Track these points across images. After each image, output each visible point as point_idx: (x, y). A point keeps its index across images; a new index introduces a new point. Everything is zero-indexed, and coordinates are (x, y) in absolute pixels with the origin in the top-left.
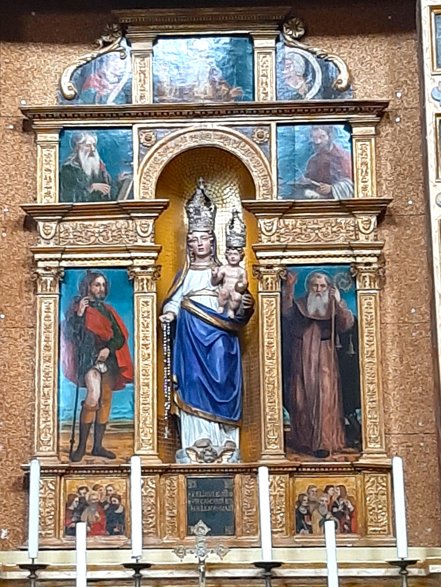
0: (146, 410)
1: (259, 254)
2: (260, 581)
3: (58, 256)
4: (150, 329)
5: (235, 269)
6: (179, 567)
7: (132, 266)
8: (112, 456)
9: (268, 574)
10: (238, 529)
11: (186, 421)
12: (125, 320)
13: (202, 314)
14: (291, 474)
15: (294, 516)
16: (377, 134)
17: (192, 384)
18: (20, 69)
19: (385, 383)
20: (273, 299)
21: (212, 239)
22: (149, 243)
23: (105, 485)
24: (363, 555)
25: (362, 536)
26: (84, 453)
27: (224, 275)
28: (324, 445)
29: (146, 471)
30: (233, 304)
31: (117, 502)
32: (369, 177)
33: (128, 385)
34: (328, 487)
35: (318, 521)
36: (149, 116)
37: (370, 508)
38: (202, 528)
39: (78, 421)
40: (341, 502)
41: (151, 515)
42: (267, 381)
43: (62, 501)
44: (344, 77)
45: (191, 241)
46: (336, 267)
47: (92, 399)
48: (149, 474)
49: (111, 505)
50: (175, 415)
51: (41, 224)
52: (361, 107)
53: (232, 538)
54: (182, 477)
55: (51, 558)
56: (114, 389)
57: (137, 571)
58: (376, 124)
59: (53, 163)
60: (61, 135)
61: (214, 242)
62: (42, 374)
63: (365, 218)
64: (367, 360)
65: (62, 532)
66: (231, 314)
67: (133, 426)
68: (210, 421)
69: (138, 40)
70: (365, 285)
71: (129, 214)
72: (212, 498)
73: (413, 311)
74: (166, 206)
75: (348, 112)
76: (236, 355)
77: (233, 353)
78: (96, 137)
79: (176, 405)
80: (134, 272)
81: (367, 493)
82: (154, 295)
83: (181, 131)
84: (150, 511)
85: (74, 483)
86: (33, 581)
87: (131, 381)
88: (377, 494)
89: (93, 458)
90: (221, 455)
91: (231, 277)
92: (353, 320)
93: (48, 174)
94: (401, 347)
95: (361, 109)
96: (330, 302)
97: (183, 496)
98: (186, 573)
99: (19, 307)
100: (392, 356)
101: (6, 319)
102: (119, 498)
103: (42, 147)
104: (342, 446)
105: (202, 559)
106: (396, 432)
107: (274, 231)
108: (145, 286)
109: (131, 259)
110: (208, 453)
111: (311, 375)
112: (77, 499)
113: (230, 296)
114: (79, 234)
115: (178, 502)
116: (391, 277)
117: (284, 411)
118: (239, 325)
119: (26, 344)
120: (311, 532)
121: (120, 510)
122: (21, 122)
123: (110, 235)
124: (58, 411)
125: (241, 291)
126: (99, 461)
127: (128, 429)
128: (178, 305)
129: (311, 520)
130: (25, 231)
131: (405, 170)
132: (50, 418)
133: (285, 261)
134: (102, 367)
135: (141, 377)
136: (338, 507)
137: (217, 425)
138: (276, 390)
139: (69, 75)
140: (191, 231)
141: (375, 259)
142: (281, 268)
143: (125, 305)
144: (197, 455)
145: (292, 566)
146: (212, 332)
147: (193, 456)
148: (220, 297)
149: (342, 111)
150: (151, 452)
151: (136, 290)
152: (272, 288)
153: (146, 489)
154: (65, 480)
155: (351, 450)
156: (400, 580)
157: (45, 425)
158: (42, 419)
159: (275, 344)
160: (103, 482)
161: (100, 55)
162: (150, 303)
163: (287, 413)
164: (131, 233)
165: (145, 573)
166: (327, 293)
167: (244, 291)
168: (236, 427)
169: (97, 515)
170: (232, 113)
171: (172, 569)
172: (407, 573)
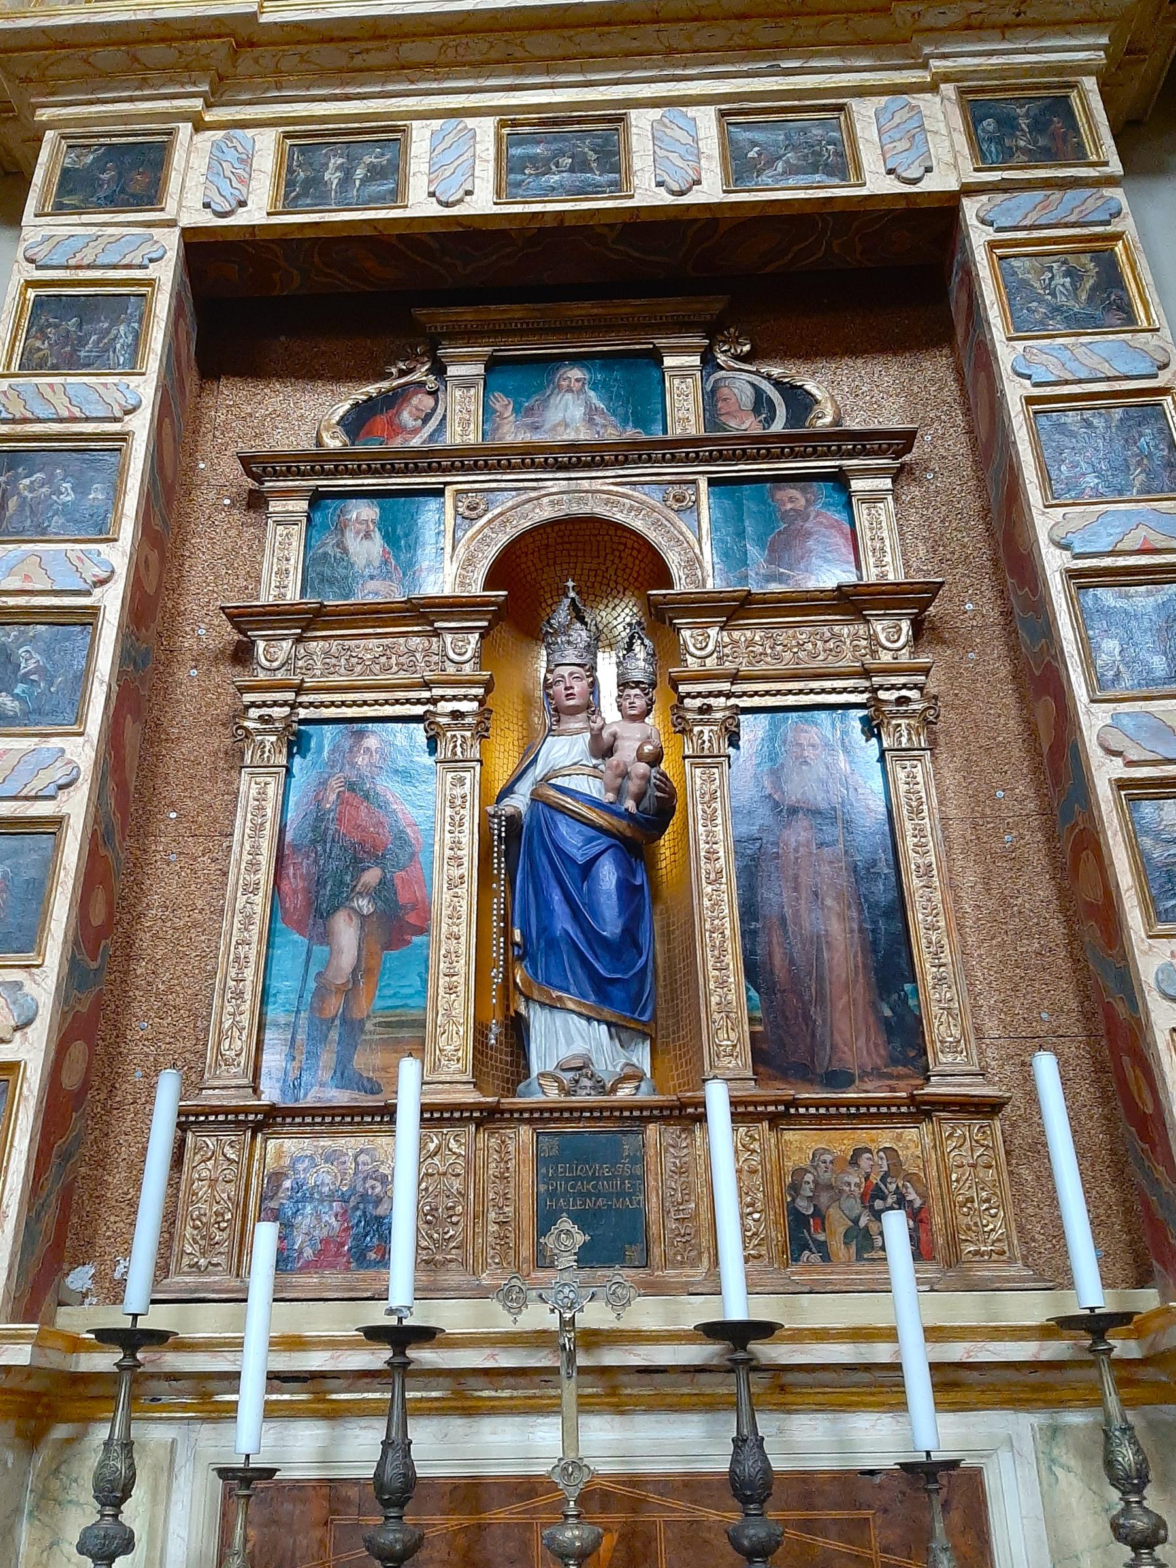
9: (741, 1355)
10: (656, 1251)
11: (539, 1021)
14: (774, 1121)
15: (784, 1221)
17: (552, 944)
20: (715, 770)
21: (591, 679)
28: (841, 1060)
30: (633, 786)
33: (416, 939)
35: (842, 1230)
36: (475, 468)
37: (961, 1198)
38: (569, 1237)
40: (893, 1187)
41: (454, 1219)
42: (708, 926)
49: (364, 1197)
51: (261, 645)
53: (641, 1274)
54: (525, 1133)
56: (388, 946)
58: (897, 475)
61: (594, 685)
66: (630, 804)
67: (422, 1025)
68: (589, 1019)
72: (594, 1177)
73: (1000, 794)
75: (841, 454)
76: (642, 885)
77: (638, 882)
78: (378, 510)
79: (521, 993)
80: (437, 724)
81: (950, 1162)
83: (534, 494)
84: (453, 1208)
87: (423, 930)
88: (974, 1166)
90: (614, 1090)
91: (629, 738)
95: (864, 446)
97: (527, 1174)
98: (530, 1356)
99: (207, 797)
100: (970, 878)
103: (278, 523)
104: (879, 1062)
106: (996, 1033)
107: (710, 648)
108: (459, 750)
109: (434, 701)
110: (586, 1082)
113: (627, 773)
114: (334, 661)
116: (947, 734)
117: (748, 990)
119: (213, 866)
120: (826, 1258)
123: (393, 661)
125: (651, 759)
128: (527, 800)
129: (824, 1230)
130: (234, 666)
131: (953, 553)
132: (246, 1007)
134: (364, 905)
135: (445, 919)
137: (604, 1027)
140: (552, 667)
141: (913, 694)
142: (727, 713)
144: (561, 1088)
145: (800, 1336)
146: (592, 839)
155: (901, 1070)
162: (468, 782)
163: (753, 993)
168: (645, 1036)
170: (626, 460)
172: (1111, 1350)
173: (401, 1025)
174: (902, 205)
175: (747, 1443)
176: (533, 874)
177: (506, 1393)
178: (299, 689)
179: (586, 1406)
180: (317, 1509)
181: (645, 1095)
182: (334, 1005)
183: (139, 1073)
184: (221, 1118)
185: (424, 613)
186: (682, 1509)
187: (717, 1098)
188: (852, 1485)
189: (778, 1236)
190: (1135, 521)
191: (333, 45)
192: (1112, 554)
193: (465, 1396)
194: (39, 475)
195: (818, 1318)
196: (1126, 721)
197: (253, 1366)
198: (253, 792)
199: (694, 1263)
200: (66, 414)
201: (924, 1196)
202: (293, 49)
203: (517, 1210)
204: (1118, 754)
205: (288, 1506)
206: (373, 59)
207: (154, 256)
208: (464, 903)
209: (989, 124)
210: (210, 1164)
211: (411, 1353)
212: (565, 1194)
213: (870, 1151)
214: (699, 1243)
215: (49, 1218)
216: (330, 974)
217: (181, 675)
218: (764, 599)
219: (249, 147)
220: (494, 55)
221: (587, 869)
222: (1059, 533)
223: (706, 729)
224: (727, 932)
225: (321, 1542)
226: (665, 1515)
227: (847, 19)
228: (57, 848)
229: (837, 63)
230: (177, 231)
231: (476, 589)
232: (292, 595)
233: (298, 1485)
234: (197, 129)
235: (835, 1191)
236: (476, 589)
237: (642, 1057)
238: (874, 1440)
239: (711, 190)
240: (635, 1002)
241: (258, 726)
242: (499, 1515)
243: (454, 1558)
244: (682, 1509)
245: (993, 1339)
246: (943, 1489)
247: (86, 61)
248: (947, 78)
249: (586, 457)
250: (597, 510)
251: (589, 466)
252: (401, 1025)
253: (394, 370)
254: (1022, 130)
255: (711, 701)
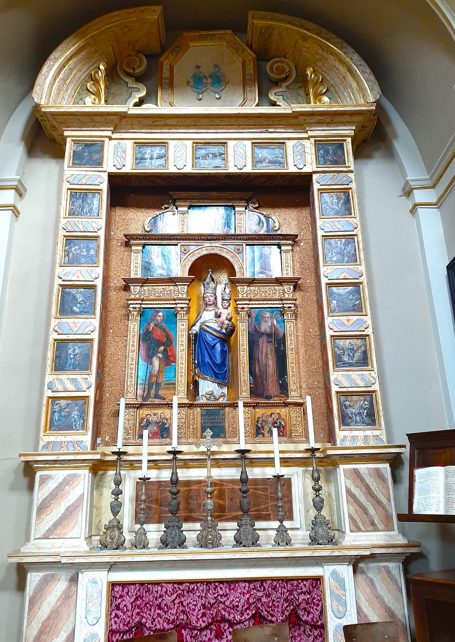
0: (181, 376)
1: (238, 302)
2: (239, 460)
3: (140, 302)
4: (184, 337)
5: (226, 310)
6: (196, 453)
7: (176, 307)
8: (164, 399)
9: (243, 456)
10: (227, 435)
11: (202, 383)
12: (172, 333)
13: (210, 330)
14: (254, 407)
15: (255, 428)
16: (292, 250)
17: (205, 364)
18: (125, 219)
19: (299, 363)
22: (184, 296)
23: (159, 413)
24: (291, 447)
25: (289, 438)
26: (150, 397)
27: (221, 313)
29: (180, 406)
30: (225, 326)
31: (166, 421)
32: (289, 269)
33: (173, 364)
34: (272, 414)
38: (209, 433)
39: (147, 381)
40: (279, 421)
43: (137, 421)
44: (277, 225)
45: (205, 298)
46: (274, 309)
47: (155, 371)
48: (182, 407)
49: (163, 423)
50: (196, 380)
51: (132, 287)
52: (285, 237)
55: (130, 450)
57: (175, 455)
58: (292, 245)
59: (139, 260)
60: (144, 247)
61: (216, 298)
62: (130, 358)
63: (288, 287)
64: (290, 352)
65: (137, 437)
66: (224, 331)
69: (181, 206)
70: (288, 316)
71: (175, 283)
73: (311, 330)
74: (193, 280)
75: (279, 239)
77: (225, 350)
82: (187, 321)
85: (144, 412)
86: (119, 461)
89: (154, 400)
90: (219, 399)
91: (224, 314)
92: (283, 333)
93: (136, 265)
94: (306, 347)
96: (272, 326)
100: (302, 351)
101: (113, 333)
102: (167, 420)
103: (134, 253)
105: (209, 449)
107: (245, 292)
108: (182, 317)
109: (176, 304)
110: (212, 397)
111: (263, 359)
112: (145, 420)
113: (224, 323)
114: (151, 292)
115: (197, 421)
118: (228, 336)
120: (264, 436)
121: (166, 426)
122: (124, 242)
123: (166, 293)
124: (137, 376)
126: (157, 401)
127: (172, 386)
128: (199, 327)
132: (133, 380)
133: (250, 306)
134: (160, 355)
135: (180, 360)
136: (277, 424)
137: (217, 384)
138: (246, 366)
139: (148, 222)
141: (293, 306)
143: (172, 326)
144: (207, 398)
145: (255, 452)
146: (215, 339)
147: (204, 399)
148: (219, 323)
149: (276, 239)
150: (183, 397)
151: (178, 319)
152: (244, 318)
153: (181, 415)
154: (139, 411)
155: (283, 395)
156: (310, 460)
157: (130, 382)
158: (129, 380)
159: (245, 344)
160: (159, 411)
161: (163, 213)
163: (251, 378)
164: (176, 292)
165: (179, 456)
166: (270, 321)
167: (230, 320)
168: (226, 386)
169: (156, 428)
170: (225, 239)
171: (193, 454)
173: (169, 384)
174: (298, 174)
175: (244, 473)
176: (200, 346)
177: (195, 464)
178: (143, 300)
179: (212, 466)
180: (156, 487)
181: (225, 401)
182: (154, 379)
183: (108, 395)
184: (130, 406)
185: (173, 281)
186: (231, 486)
187: (241, 404)
188: (265, 481)
189: (254, 432)
190: (343, 271)
191: (147, 119)
192: (337, 279)
193: (187, 464)
194: (77, 247)
195: (259, 449)
196: (334, 321)
197: (145, 458)
198: (132, 327)
199: (235, 437)
200: (83, 230)
201: (285, 423)
202: (137, 119)
203: (197, 426)
204: (332, 329)
205: (150, 486)
206: (159, 123)
207: (102, 182)
208: (184, 356)
209: (322, 152)
210: (128, 416)
211: (177, 456)
212: (208, 422)
213: (274, 413)
214: (236, 433)
215: (95, 429)
216: (152, 372)
217: (111, 294)
218: (258, 280)
219: (125, 147)
220: (192, 124)
221: (213, 347)
222: (326, 273)
223: (243, 313)
224: (246, 364)
225: (157, 493)
226: (227, 487)
227: (287, 119)
228: (92, 346)
229: (284, 131)
230: (106, 174)
231: (186, 275)
232: (139, 276)
233: (152, 482)
234: (110, 140)
235: (267, 422)
236: (186, 275)
237: (225, 390)
238: (269, 472)
239: (248, 169)
240: (224, 378)
241: (133, 309)
242: (194, 487)
243: (185, 495)
244: (231, 486)
245: (294, 453)
246: (284, 483)
247: (79, 120)
248: (312, 137)
249: (215, 237)
250: (217, 252)
251: (215, 240)
252: (169, 384)
253: (163, 207)
254: (330, 154)
255: (244, 306)
